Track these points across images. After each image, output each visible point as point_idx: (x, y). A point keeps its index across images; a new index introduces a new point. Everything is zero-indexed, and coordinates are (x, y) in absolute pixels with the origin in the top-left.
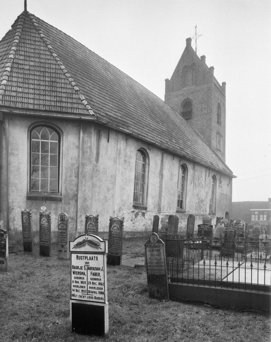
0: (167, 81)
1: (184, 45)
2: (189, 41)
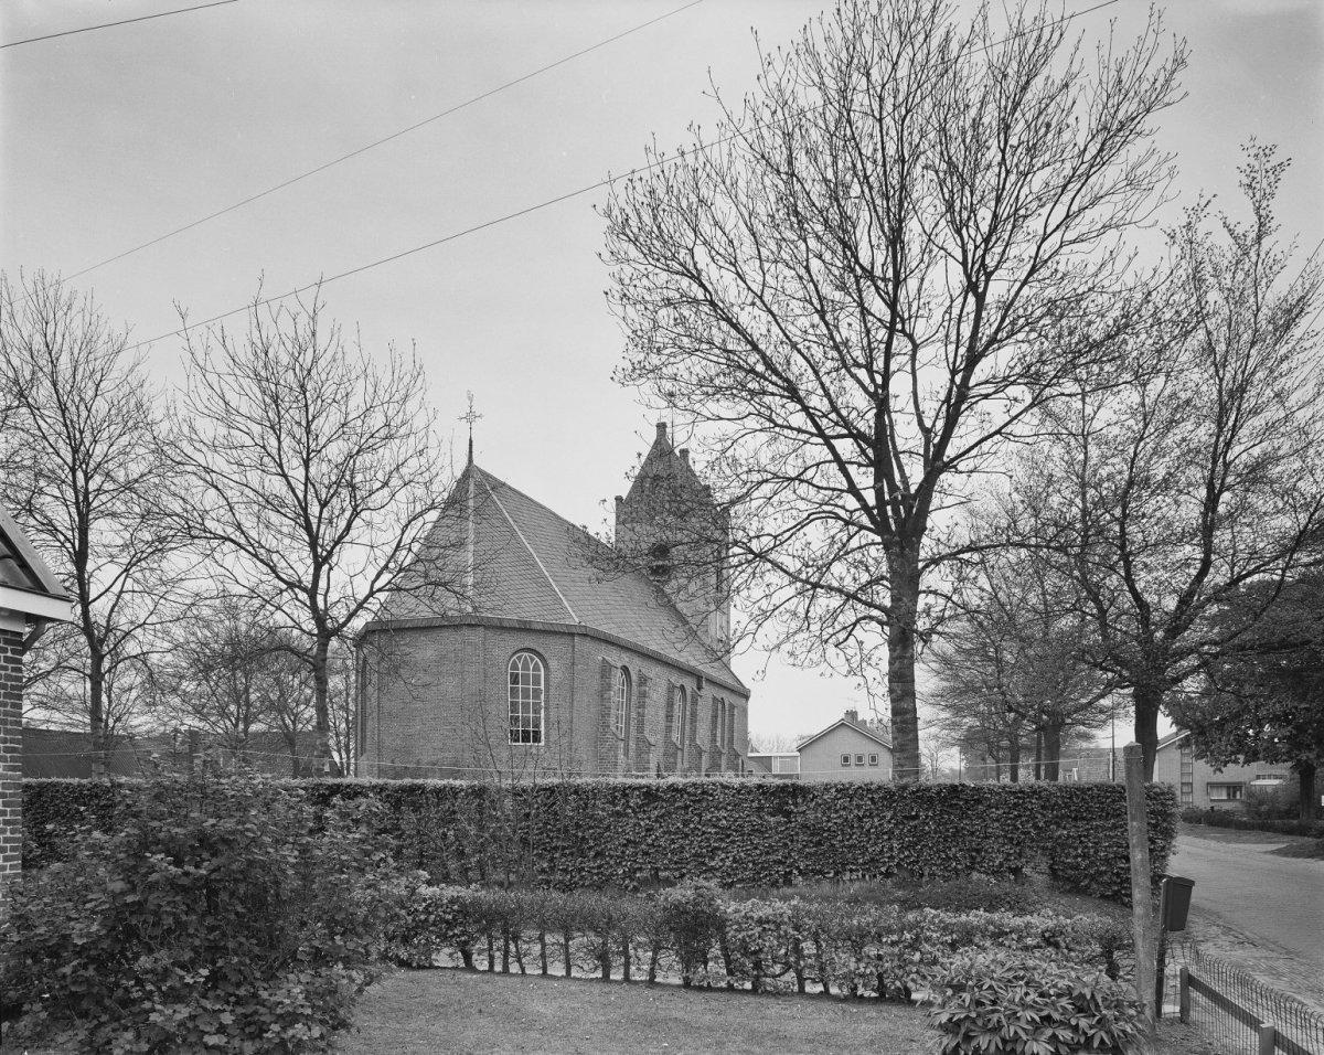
0: (618, 499)
1: (652, 436)
2: (661, 427)
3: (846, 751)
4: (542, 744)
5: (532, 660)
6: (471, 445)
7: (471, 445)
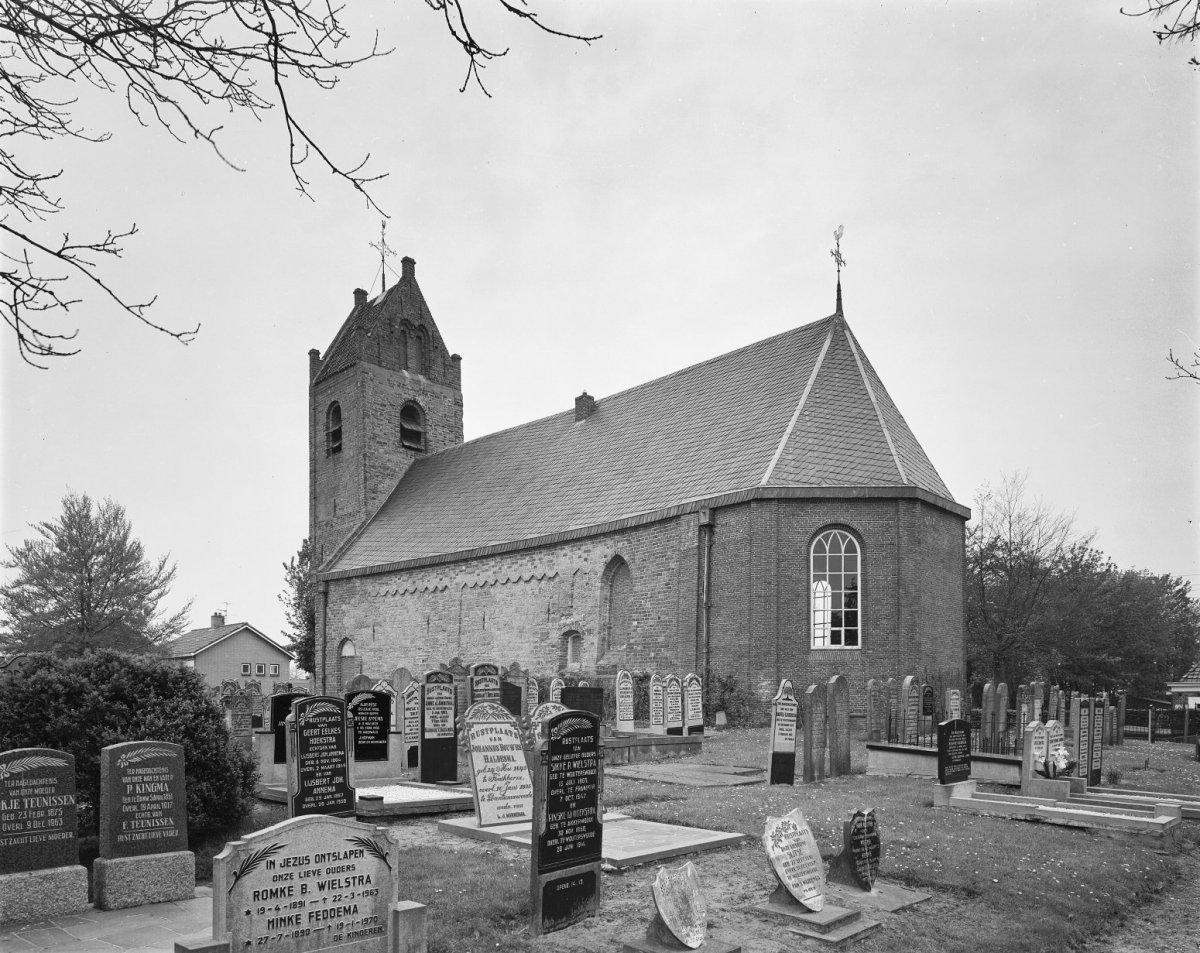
3: (248, 659)
4: (859, 646)
5: (844, 538)
6: (839, 291)
7: (839, 291)
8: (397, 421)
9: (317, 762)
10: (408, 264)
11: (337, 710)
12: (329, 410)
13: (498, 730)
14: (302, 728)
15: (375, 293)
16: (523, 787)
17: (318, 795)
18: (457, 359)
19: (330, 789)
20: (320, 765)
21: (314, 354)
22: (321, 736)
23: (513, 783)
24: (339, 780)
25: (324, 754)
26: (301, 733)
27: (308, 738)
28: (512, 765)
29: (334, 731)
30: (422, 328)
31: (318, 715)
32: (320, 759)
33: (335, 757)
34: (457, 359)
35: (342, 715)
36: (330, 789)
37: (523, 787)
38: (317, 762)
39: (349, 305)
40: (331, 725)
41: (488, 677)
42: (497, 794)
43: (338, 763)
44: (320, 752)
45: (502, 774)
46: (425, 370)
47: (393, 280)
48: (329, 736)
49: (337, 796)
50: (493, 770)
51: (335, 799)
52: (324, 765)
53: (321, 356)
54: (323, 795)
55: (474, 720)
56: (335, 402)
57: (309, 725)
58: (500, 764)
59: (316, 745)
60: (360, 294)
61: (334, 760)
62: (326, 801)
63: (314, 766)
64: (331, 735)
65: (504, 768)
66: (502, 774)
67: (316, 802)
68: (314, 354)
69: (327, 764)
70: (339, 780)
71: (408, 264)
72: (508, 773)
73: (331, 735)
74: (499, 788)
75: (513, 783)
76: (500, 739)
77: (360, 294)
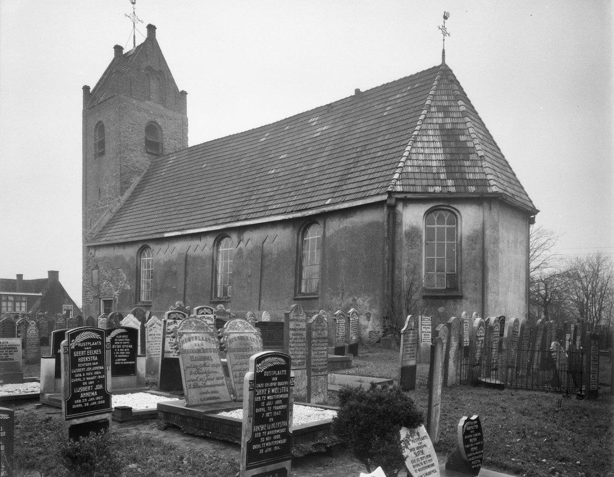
8: (143, 136)
9: (84, 375)
10: (151, 29)
11: (98, 336)
12: (97, 124)
13: (201, 338)
14: (73, 351)
15: (128, 48)
16: (218, 379)
17: (85, 398)
18: (184, 93)
19: (93, 394)
20: (86, 376)
21: (86, 88)
22: (86, 356)
23: (211, 375)
24: (99, 387)
25: (89, 369)
26: (72, 354)
27: (77, 358)
28: (211, 363)
29: (96, 352)
30: (161, 72)
31: (85, 341)
32: (85, 372)
33: (97, 370)
34: (184, 93)
35: (102, 341)
36: (93, 394)
37: (218, 379)
38: (84, 375)
39: (111, 56)
40: (94, 348)
41: (206, 316)
42: (200, 383)
43: (99, 375)
44: (86, 367)
45: (204, 369)
46: (163, 101)
47: (141, 38)
48: (92, 355)
49: (98, 398)
50: (195, 367)
51: (97, 401)
52: (88, 376)
53: (91, 90)
54: (88, 398)
55: (229, 331)
56: (100, 122)
57: (78, 348)
58: (202, 362)
59: (83, 363)
60: (118, 49)
61: (97, 373)
62: (90, 402)
63: (82, 378)
64: (95, 355)
65: (205, 365)
66: (204, 369)
67: (83, 404)
68: (86, 88)
69: (91, 376)
70: (99, 387)
71: (151, 29)
72: (208, 368)
73: (95, 355)
74: (201, 380)
75: (211, 375)
76: (202, 345)
77: (118, 49)
